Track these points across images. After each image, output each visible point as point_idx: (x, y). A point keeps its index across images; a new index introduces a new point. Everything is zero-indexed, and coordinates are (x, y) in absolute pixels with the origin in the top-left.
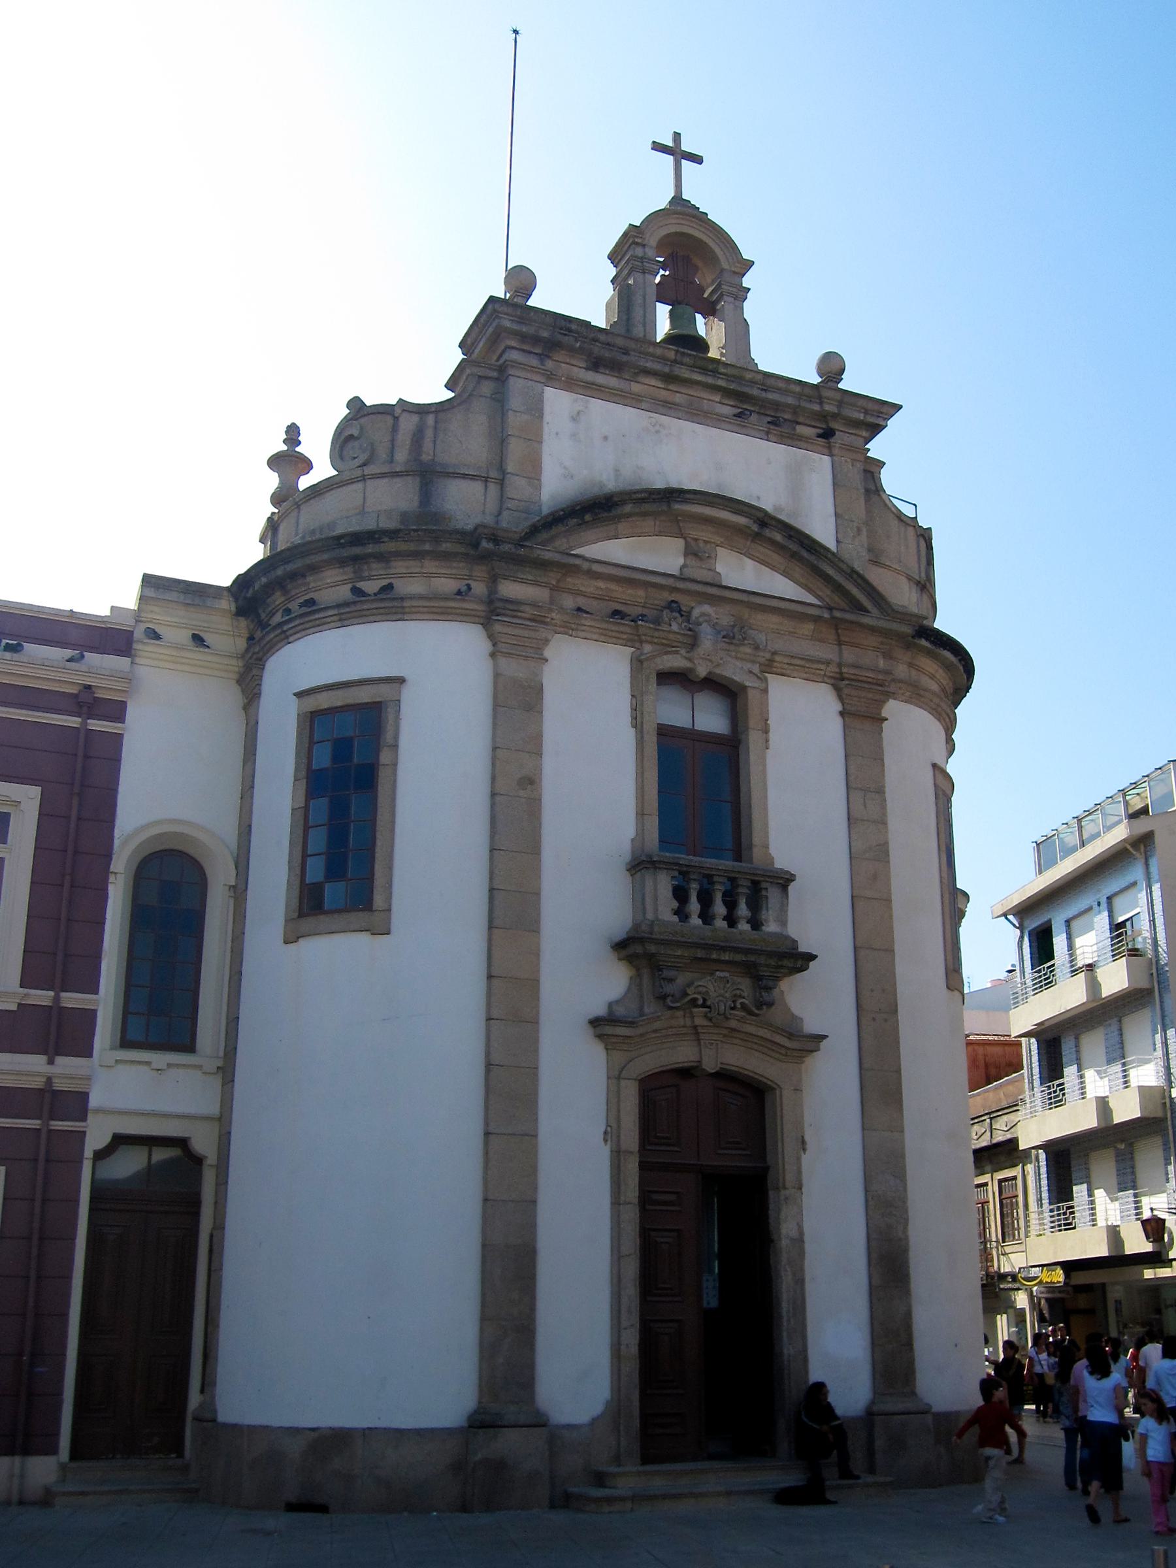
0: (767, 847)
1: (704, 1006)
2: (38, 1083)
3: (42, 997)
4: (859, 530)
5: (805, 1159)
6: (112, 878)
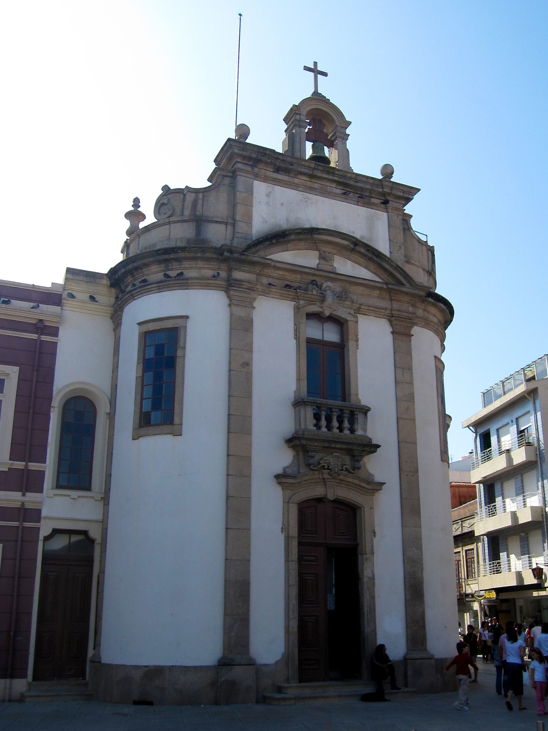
0: (357, 395)
1: (328, 469)
2: (18, 505)
3: (19, 465)
4: (400, 247)
5: (375, 540)
6: (52, 410)
